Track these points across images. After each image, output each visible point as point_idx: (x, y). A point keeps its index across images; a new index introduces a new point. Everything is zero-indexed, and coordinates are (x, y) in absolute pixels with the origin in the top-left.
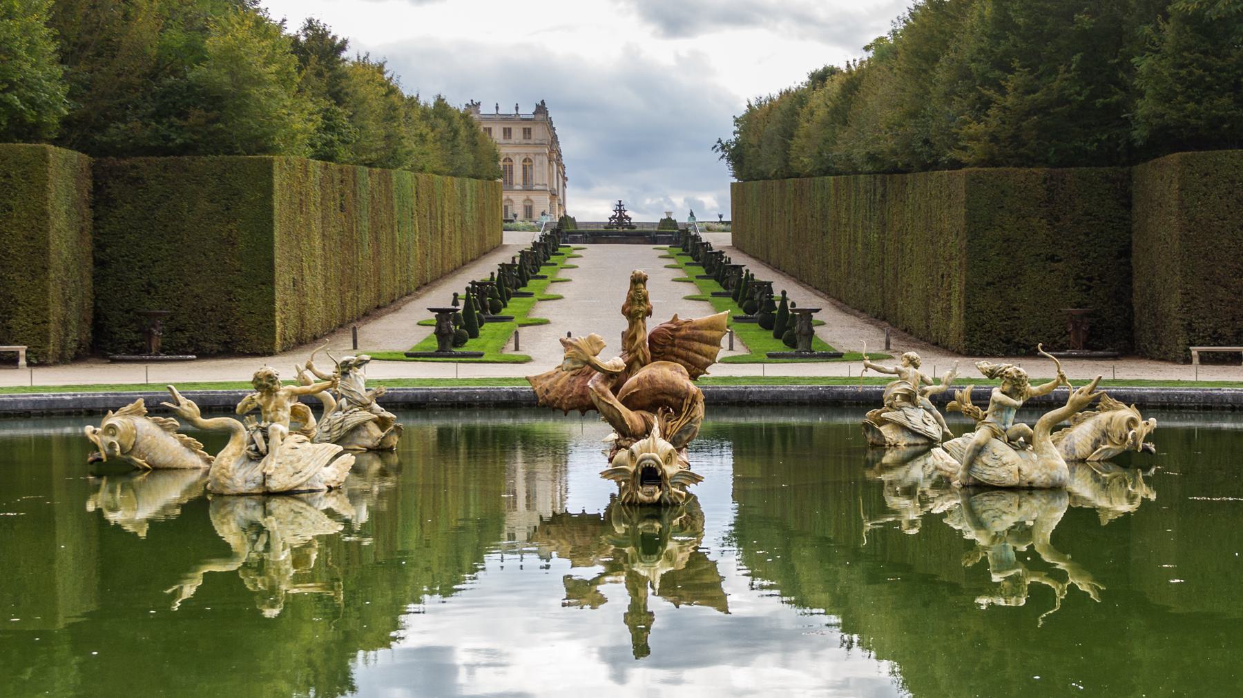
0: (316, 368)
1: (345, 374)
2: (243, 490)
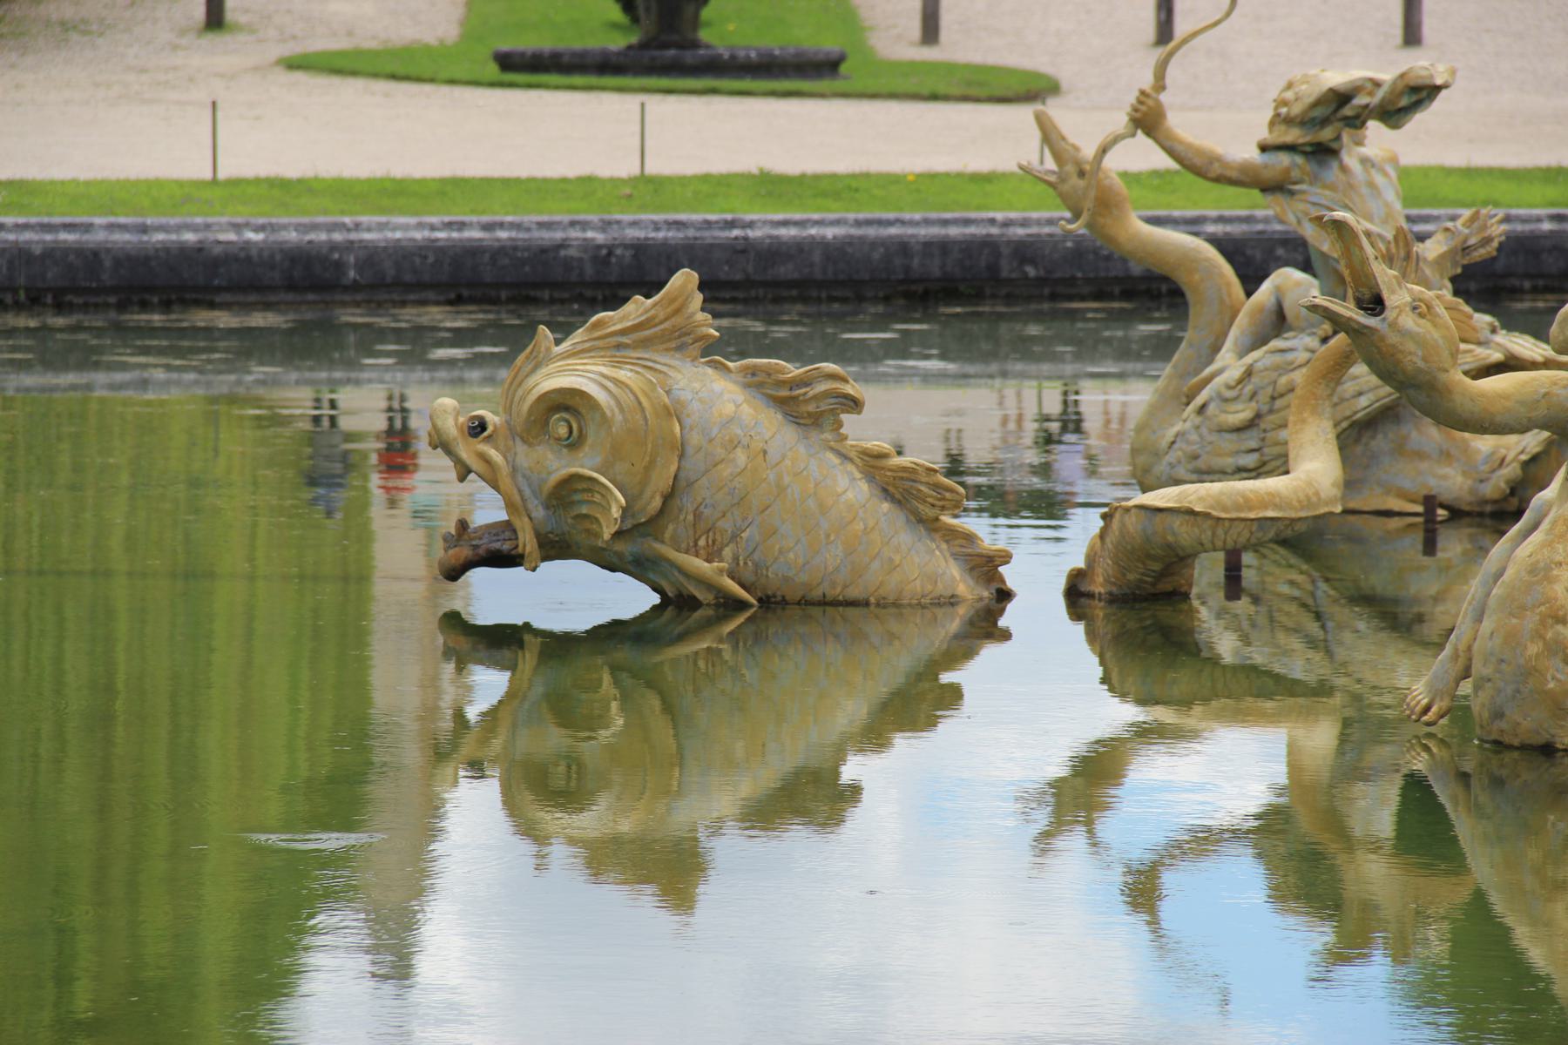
0: (1180, 123)
1: (1323, 153)
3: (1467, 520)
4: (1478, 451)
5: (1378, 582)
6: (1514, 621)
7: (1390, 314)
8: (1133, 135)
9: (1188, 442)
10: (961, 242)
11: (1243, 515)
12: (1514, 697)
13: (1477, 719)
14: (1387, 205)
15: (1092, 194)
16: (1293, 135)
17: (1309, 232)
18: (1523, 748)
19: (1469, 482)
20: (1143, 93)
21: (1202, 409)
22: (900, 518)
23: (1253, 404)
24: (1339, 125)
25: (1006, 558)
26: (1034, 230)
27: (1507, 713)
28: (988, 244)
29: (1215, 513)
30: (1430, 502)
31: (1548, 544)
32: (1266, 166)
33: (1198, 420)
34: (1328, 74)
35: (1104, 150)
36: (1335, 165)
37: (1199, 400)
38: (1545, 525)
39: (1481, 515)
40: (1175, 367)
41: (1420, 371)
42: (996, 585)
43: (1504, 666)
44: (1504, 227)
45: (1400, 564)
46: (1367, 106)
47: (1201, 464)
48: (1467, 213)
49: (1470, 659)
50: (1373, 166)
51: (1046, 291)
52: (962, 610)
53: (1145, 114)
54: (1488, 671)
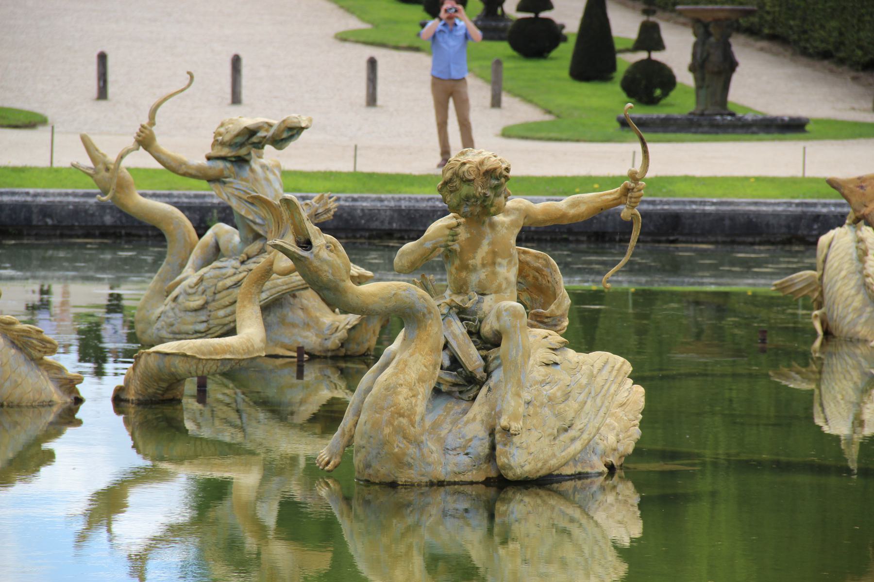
0: (162, 142)
1: (241, 161)
2: (441, 472)
3: (318, 360)
4: (324, 323)
5: (271, 393)
6: (377, 415)
7: (315, 250)
8: (138, 149)
9: (168, 317)
10: (10, 205)
11: (213, 357)
12: (376, 457)
13: (357, 469)
14: (276, 190)
15: (115, 181)
16: (225, 152)
17: (234, 203)
18: (381, 484)
19: (320, 340)
20: (142, 126)
21: (175, 299)
22: (21, 358)
23: (204, 296)
24: (250, 146)
25: (80, 380)
26: (51, 199)
27: (373, 465)
28: (25, 206)
29: (198, 356)
30: (300, 350)
31: (395, 374)
32: (210, 168)
33: (173, 305)
34: (244, 119)
35: (121, 157)
36: (248, 168)
37: (174, 294)
38: (393, 364)
39: (325, 357)
40: (159, 276)
41: (330, 280)
42: (74, 395)
43: (371, 439)
44: (337, 204)
45: (283, 383)
46: (265, 137)
47: (174, 329)
48: (317, 196)
49: (352, 437)
50: (268, 169)
51: (58, 232)
52: (55, 409)
53: (144, 138)
54: (363, 443)
